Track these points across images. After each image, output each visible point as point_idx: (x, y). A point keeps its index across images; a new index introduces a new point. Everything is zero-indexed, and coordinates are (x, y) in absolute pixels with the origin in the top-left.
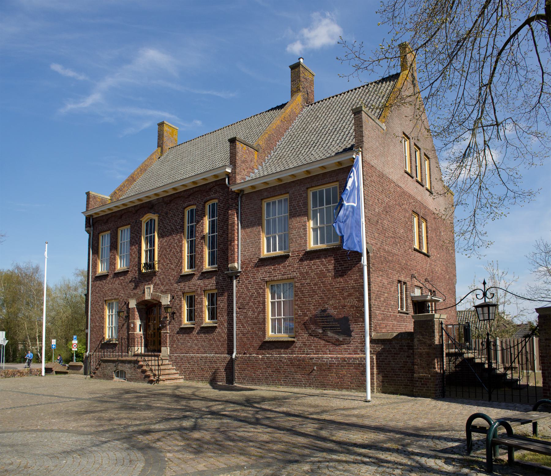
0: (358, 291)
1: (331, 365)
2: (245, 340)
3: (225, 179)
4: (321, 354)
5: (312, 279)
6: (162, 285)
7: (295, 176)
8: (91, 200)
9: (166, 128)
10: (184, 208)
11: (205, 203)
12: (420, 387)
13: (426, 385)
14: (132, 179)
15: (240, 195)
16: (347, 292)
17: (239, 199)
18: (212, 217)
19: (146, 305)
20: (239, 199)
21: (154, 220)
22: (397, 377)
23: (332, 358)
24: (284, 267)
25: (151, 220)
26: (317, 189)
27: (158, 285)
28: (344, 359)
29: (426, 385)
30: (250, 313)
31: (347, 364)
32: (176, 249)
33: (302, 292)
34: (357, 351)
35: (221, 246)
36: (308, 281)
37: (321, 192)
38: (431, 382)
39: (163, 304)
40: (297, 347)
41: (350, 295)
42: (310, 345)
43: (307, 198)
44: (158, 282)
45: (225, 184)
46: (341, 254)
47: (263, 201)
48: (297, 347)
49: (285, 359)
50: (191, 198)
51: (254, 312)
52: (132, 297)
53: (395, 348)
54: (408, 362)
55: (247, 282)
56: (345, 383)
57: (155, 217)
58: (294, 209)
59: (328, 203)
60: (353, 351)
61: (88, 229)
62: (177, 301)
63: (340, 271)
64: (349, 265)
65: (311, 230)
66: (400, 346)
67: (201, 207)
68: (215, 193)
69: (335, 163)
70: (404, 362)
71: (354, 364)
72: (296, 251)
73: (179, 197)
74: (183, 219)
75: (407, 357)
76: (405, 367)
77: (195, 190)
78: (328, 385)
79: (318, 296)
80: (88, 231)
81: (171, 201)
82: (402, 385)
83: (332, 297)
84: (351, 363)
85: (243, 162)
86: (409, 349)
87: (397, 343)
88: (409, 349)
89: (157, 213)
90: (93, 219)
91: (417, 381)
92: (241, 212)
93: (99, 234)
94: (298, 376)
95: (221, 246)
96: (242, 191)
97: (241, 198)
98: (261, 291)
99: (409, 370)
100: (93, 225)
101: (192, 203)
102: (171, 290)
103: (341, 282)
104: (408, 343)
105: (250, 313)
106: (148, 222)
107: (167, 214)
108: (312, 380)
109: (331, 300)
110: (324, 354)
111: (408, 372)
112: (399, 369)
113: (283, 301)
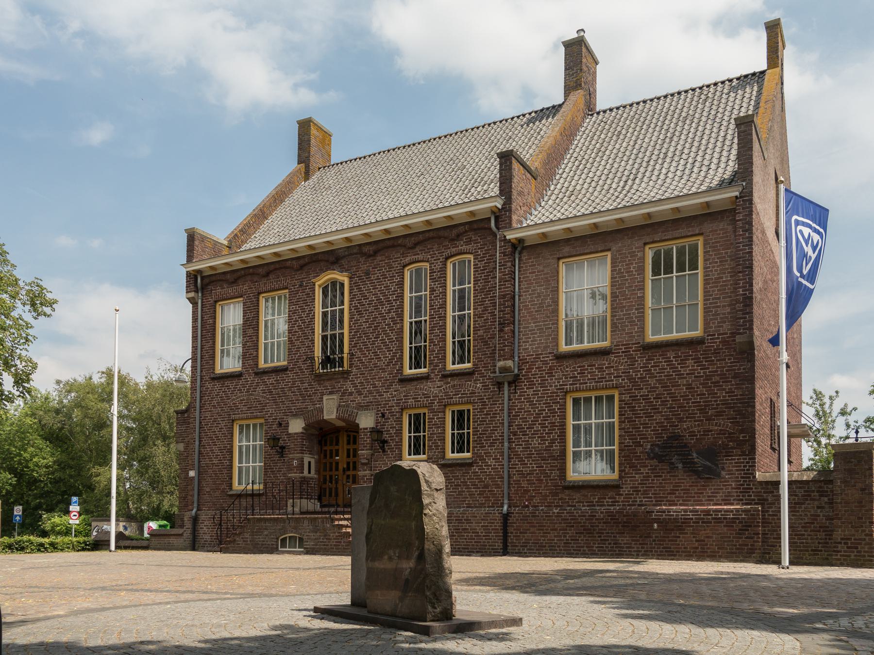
0: (731, 408)
1: (686, 521)
2: (524, 484)
3: (489, 219)
4: (665, 505)
5: (653, 389)
6: (360, 393)
7: (679, 211)
8: (196, 243)
9: (313, 131)
10: (404, 266)
11: (447, 258)
12: (845, 552)
13: (857, 548)
14: (261, 215)
15: (519, 249)
16: (713, 409)
17: (517, 256)
18: (460, 284)
19: (321, 429)
20: (517, 256)
21: (342, 285)
22: (799, 539)
23: (685, 511)
24: (600, 369)
25: (334, 283)
26: (663, 246)
27: (351, 394)
28: (707, 512)
29: (857, 548)
30: (535, 442)
31: (713, 519)
32: (388, 335)
33: (633, 409)
34: (730, 500)
35: (481, 333)
36: (644, 391)
37: (669, 253)
38: (865, 544)
39: (361, 426)
40: (622, 495)
41: (719, 414)
42: (645, 493)
43: (643, 259)
44: (351, 389)
45: (490, 229)
46: (705, 351)
47: (647, 247)
48: (622, 495)
49: (602, 513)
50: (417, 249)
51: (542, 438)
52: (295, 416)
53: (796, 495)
54: (819, 516)
55: (531, 392)
56: (708, 548)
57: (344, 278)
58: (620, 277)
59: (681, 268)
60: (723, 500)
61: (192, 295)
62: (391, 421)
63: (702, 376)
64: (718, 367)
65: (650, 312)
66: (805, 491)
67: (439, 265)
68: (468, 243)
69: (538, 234)
70: (811, 515)
71: (725, 518)
72: (623, 345)
73: (393, 246)
74: (401, 284)
75: (818, 507)
76: (813, 523)
77: (427, 235)
78: (678, 552)
79: (662, 416)
80: (192, 300)
81: (376, 253)
82: (807, 551)
83: (687, 418)
84: (720, 518)
85: (520, 193)
86: (821, 496)
87: (800, 488)
88: (821, 496)
89: (346, 271)
90: (203, 278)
91: (840, 543)
92: (519, 278)
93: (216, 302)
94: (624, 540)
95: (481, 333)
96: (521, 241)
97: (520, 253)
98: (556, 407)
99: (820, 527)
100: (202, 289)
101: (420, 257)
102: (378, 404)
103: (704, 394)
104: (820, 487)
105: (535, 442)
106: (327, 287)
107: (367, 273)
108: (651, 544)
109: (685, 422)
110: (670, 505)
111: (819, 531)
112: (803, 527)
113: (597, 425)
